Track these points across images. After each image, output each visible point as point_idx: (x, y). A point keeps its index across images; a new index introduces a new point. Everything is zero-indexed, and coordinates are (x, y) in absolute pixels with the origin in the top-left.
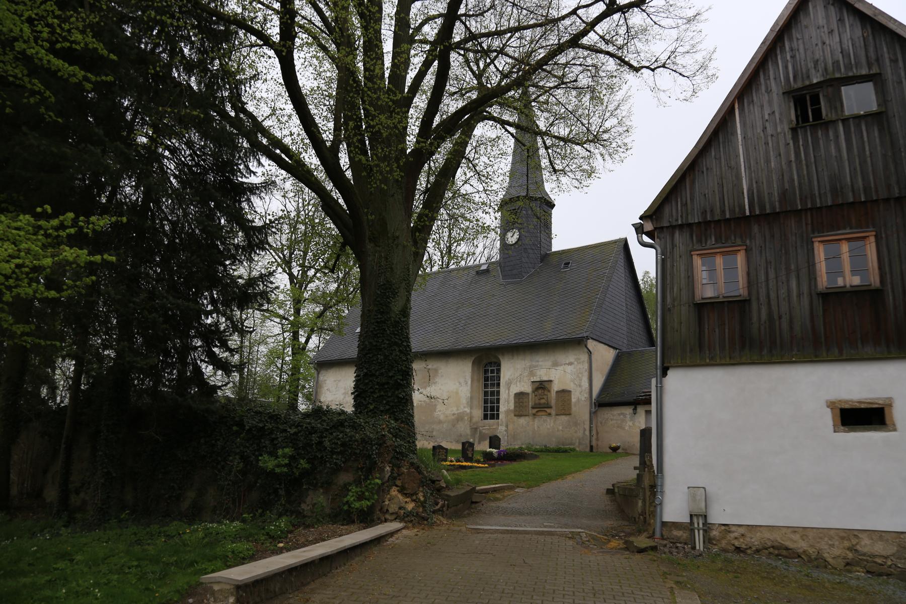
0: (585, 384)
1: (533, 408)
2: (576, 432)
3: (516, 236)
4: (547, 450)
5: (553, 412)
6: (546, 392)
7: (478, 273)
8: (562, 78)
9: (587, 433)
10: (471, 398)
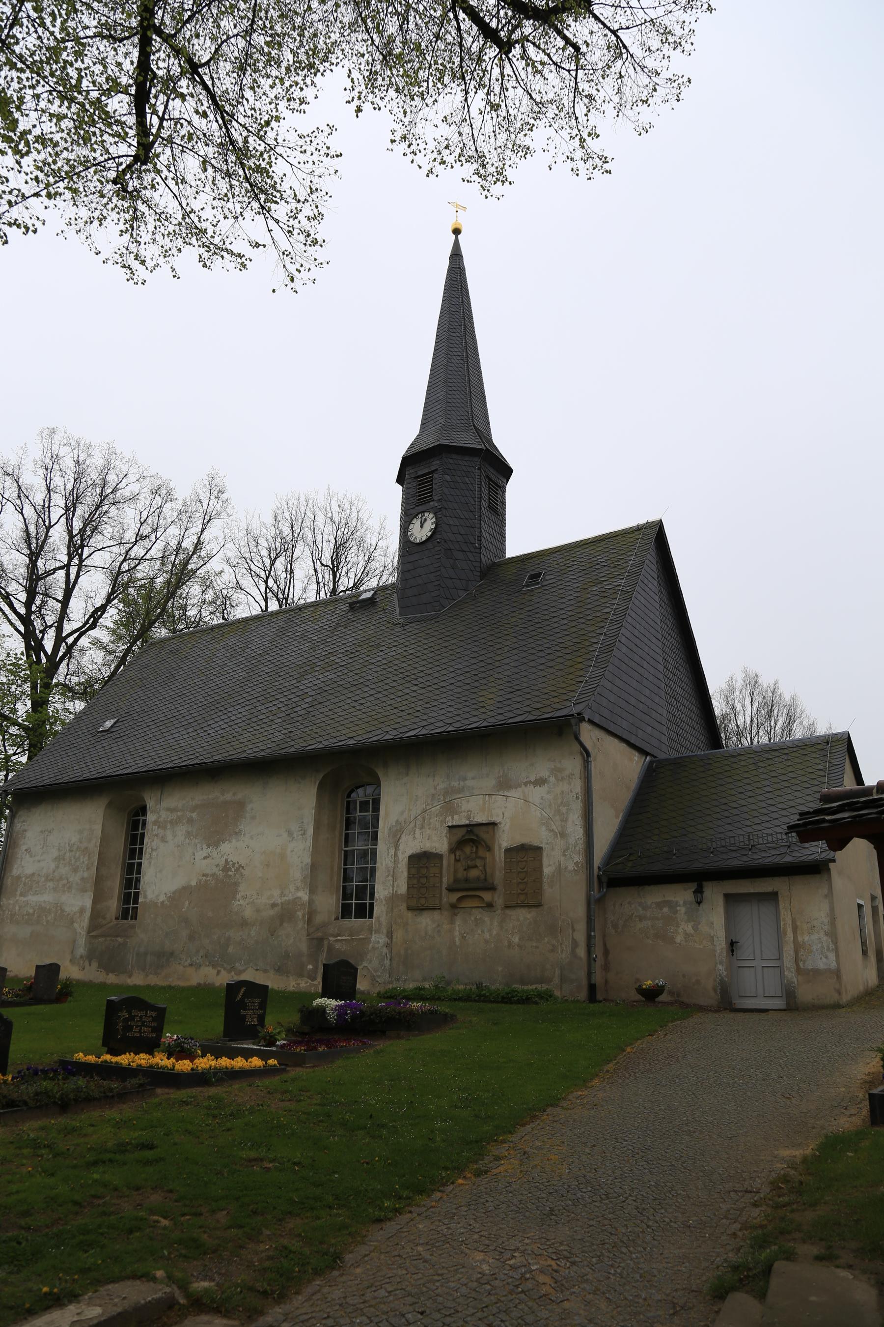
0: (576, 830)
1: (450, 890)
2: (553, 950)
3: (430, 525)
4: (480, 997)
5: (499, 900)
6: (482, 852)
7: (352, 607)
8: (631, 1253)
9: (582, 952)
10: (314, 867)
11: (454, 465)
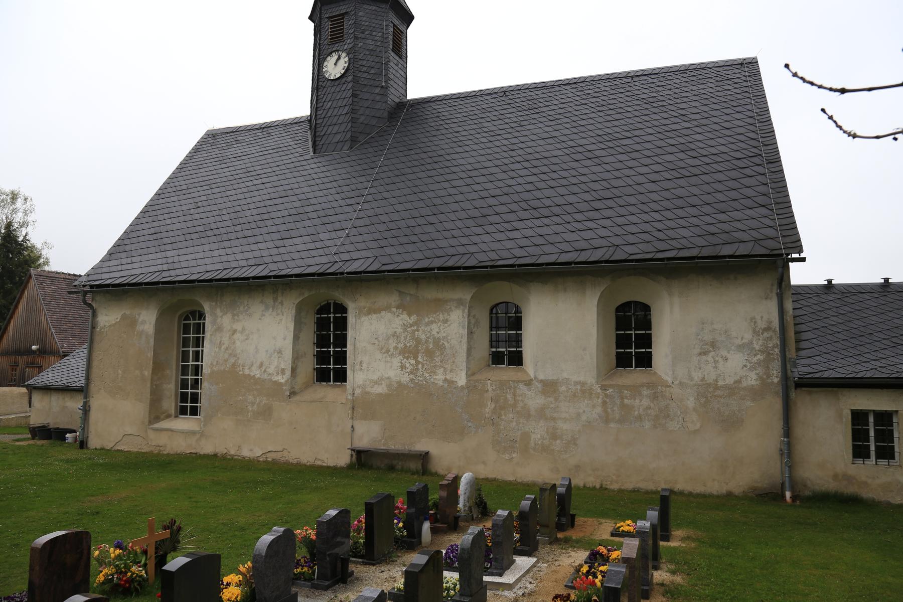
3: (343, 63)
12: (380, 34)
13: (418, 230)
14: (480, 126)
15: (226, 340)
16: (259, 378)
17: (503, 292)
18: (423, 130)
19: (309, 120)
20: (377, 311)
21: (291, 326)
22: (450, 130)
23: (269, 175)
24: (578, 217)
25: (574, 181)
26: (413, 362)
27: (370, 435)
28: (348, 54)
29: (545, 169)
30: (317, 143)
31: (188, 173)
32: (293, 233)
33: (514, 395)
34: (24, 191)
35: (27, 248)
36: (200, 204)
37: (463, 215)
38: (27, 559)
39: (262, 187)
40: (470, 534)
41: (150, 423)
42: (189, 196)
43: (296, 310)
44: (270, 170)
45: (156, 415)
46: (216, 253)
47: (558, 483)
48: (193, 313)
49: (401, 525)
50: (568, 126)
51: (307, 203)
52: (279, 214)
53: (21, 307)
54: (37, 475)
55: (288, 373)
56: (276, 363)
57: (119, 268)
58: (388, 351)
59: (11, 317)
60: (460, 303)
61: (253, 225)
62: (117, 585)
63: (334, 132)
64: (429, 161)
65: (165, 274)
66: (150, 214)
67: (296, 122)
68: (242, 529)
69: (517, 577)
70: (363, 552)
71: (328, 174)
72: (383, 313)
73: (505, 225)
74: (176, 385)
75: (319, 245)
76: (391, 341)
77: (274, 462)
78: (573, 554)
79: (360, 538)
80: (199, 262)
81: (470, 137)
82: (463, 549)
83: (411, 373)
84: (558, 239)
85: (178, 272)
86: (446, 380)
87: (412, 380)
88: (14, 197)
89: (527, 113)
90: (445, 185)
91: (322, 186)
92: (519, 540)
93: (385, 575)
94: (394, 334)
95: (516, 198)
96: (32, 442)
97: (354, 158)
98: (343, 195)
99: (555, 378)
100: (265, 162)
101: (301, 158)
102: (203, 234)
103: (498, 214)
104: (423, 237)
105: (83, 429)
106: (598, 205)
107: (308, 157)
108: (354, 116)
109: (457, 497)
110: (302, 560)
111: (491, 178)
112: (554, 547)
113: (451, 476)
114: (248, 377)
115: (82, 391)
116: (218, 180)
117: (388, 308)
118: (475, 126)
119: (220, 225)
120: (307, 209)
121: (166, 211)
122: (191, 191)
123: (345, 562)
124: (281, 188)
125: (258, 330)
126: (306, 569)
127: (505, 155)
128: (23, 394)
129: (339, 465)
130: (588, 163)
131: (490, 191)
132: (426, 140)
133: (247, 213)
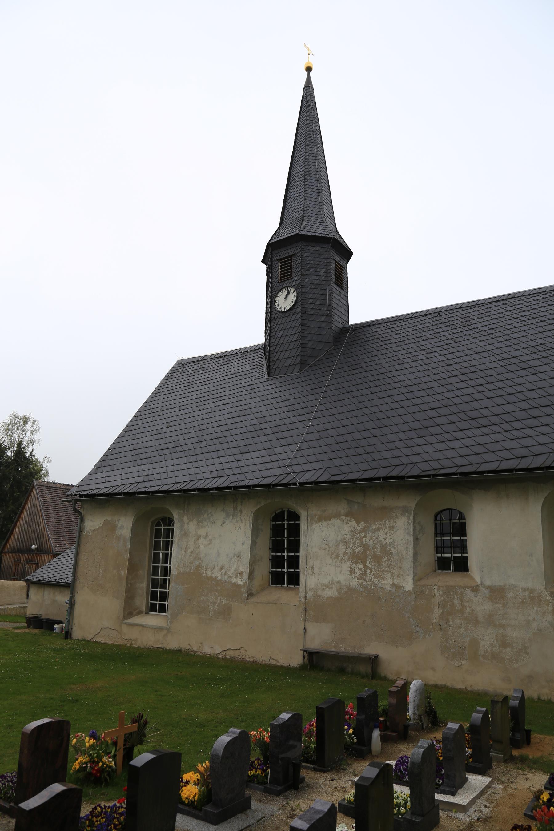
3: (292, 297)
11: (306, 253)
12: (323, 270)
13: (363, 443)
14: (417, 344)
15: (191, 544)
16: (220, 580)
17: (446, 499)
18: (365, 352)
19: (264, 347)
20: (328, 518)
21: (250, 533)
22: (390, 350)
23: (230, 396)
24: (517, 425)
25: (510, 390)
26: (361, 567)
27: (321, 636)
28: (296, 289)
29: (481, 381)
30: (271, 367)
31: (161, 397)
32: (251, 448)
33: (461, 600)
34: (34, 416)
35: (32, 462)
36: (171, 424)
37: (405, 427)
38: (18, 741)
39: (224, 407)
40: (421, 747)
41: (125, 618)
42: (162, 417)
43: (254, 517)
44: (231, 392)
45: (129, 611)
46: (184, 467)
47: (510, 693)
48: (164, 519)
49: (351, 731)
50: (501, 339)
51: (262, 420)
52: (239, 431)
53: (25, 512)
54: (30, 661)
55: (246, 576)
56: (235, 567)
57: (104, 480)
58: (337, 557)
59: (17, 521)
60: (405, 510)
61: (216, 441)
62: (90, 774)
63: (286, 356)
64: (372, 378)
65: (141, 485)
66: (130, 433)
67: (252, 350)
68: (201, 725)
69: (471, 798)
70: (315, 757)
71: (281, 394)
72: (333, 520)
73: (446, 436)
74: (148, 585)
75: (274, 458)
76: (340, 547)
77: (232, 660)
78: (530, 776)
79: (312, 742)
80: (170, 475)
81: (409, 355)
82: (413, 763)
83: (359, 578)
84: (498, 447)
85: (152, 483)
86: (393, 585)
87: (361, 584)
88: (26, 420)
89: (461, 330)
90: (388, 400)
91: (276, 406)
92: (472, 756)
93: (335, 784)
94: (344, 540)
95: (454, 409)
96: (27, 630)
97: (304, 379)
98: (294, 413)
99: (502, 584)
100: (226, 385)
101: (257, 381)
102: (173, 450)
103: (438, 425)
104: (369, 449)
105: (69, 621)
106: (536, 412)
107: (263, 380)
108: (303, 342)
109: (406, 704)
110: (256, 762)
111: (430, 392)
112: (510, 766)
113: (400, 683)
114: (211, 578)
115: (69, 587)
116: (186, 403)
117: (337, 516)
118: (412, 345)
119: (188, 442)
120: (263, 426)
121: (143, 430)
122: (163, 412)
123: (297, 768)
124: (240, 408)
125: (220, 536)
126: (259, 772)
127: (443, 370)
128: (23, 587)
129: (292, 666)
130: (523, 373)
131: (430, 404)
132: (368, 360)
133: (211, 431)
